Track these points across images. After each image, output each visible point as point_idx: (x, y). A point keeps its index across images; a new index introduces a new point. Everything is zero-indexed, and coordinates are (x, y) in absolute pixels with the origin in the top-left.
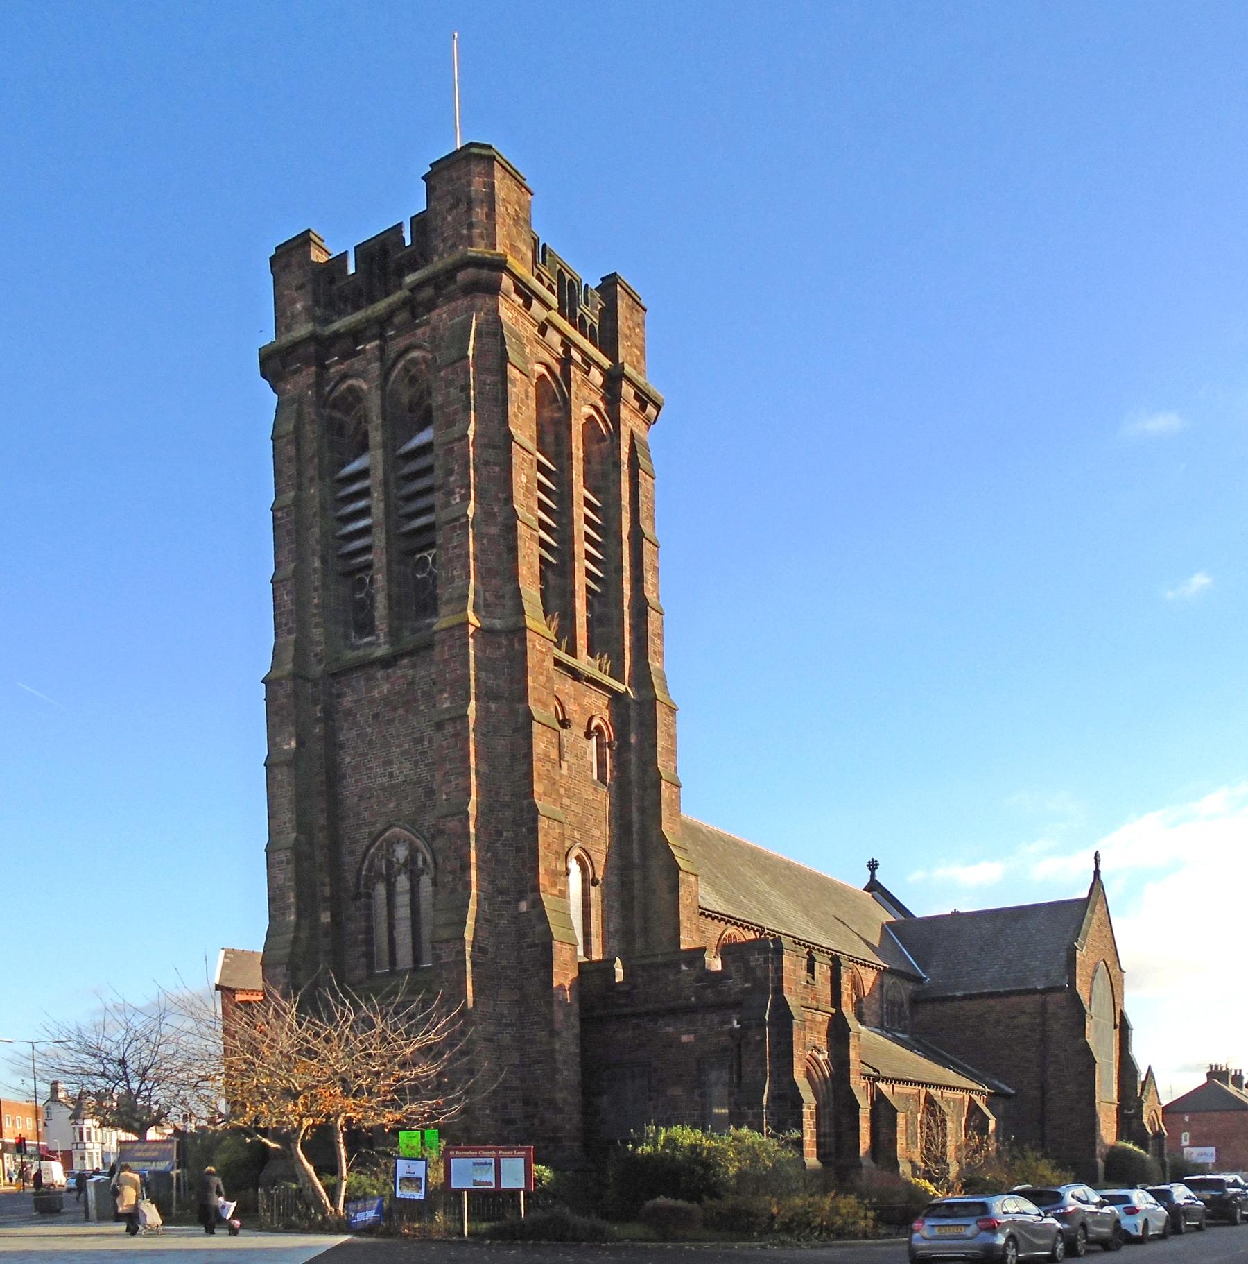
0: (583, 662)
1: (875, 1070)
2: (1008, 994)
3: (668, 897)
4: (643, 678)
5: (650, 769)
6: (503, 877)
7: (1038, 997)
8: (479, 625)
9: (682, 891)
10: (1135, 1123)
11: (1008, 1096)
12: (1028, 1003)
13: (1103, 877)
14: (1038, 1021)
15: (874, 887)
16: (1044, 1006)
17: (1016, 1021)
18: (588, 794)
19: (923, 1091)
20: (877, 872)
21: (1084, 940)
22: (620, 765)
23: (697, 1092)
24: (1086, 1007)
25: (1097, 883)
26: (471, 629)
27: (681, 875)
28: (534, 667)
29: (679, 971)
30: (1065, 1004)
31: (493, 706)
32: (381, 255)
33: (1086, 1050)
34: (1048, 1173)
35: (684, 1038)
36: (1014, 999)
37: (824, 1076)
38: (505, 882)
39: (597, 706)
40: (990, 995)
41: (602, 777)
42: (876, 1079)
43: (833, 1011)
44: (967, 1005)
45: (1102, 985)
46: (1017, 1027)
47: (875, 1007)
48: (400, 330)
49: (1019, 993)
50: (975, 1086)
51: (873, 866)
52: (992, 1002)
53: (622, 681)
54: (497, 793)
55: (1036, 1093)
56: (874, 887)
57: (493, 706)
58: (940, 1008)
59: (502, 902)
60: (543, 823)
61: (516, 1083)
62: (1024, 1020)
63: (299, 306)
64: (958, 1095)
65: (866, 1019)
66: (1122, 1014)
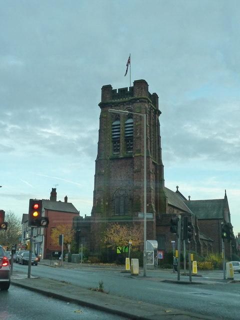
12: (215, 221)
15: (178, 192)
25: (226, 197)
32: (123, 91)
48: (127, 104)
51: (177, 187)
63: (107, 96)
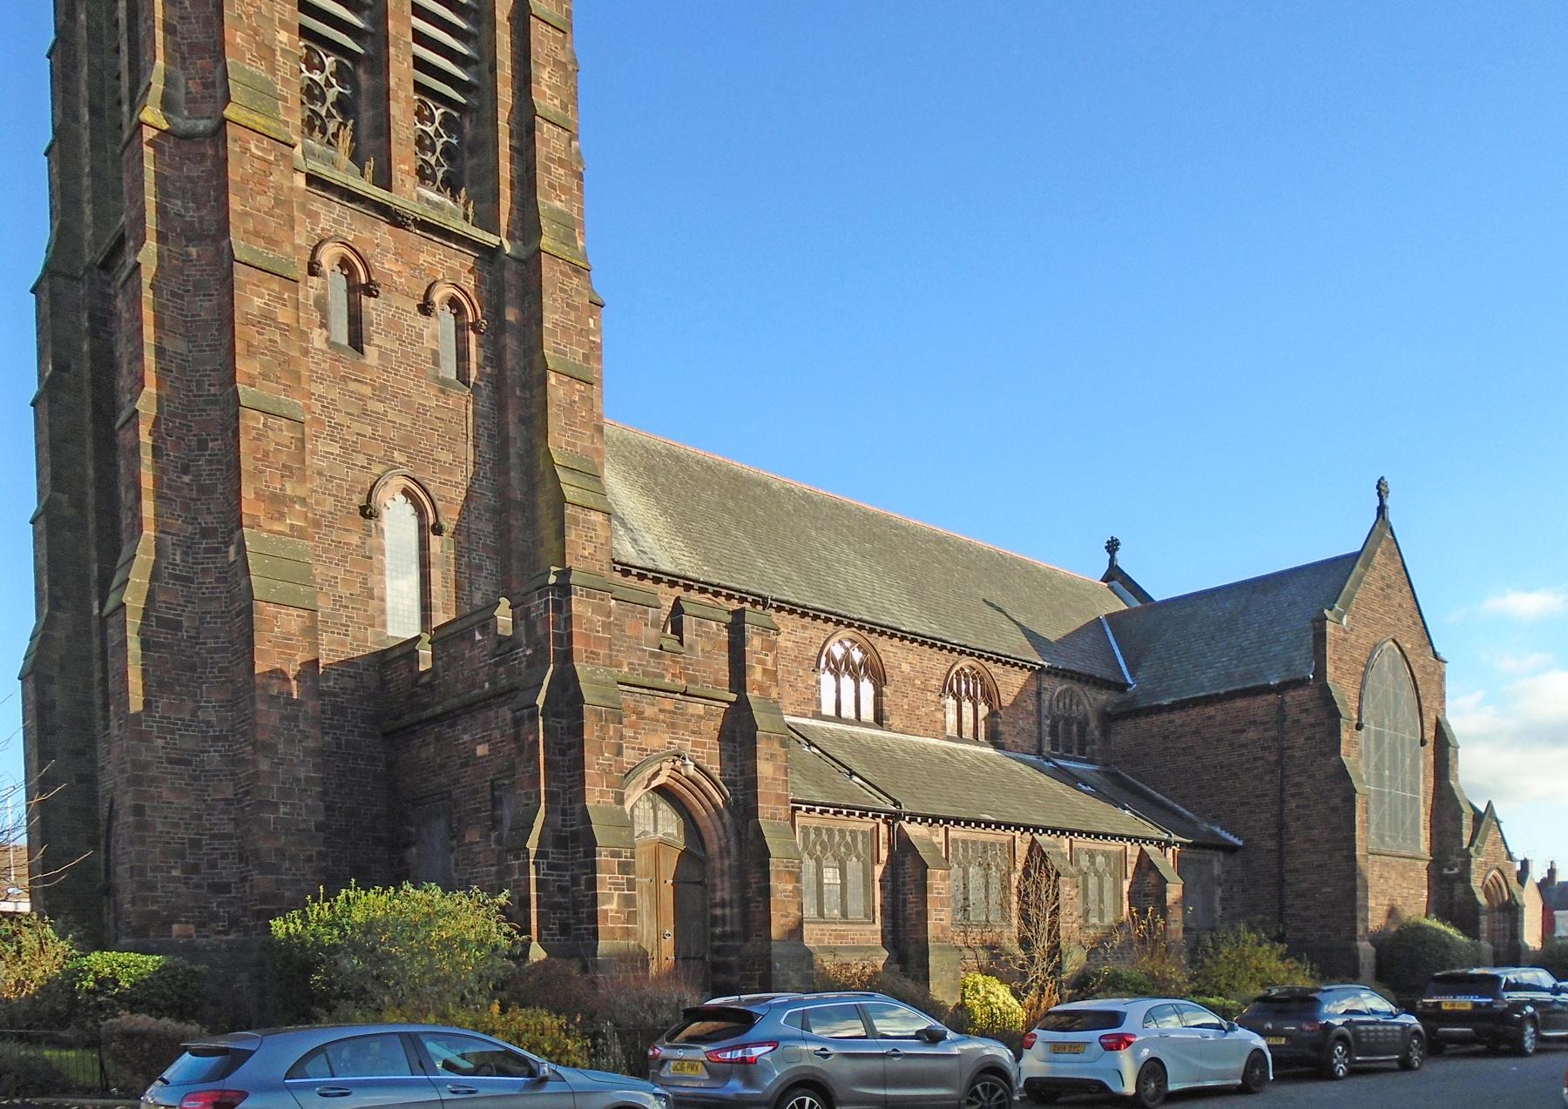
0: (410, 194)
1: (896, 803)
2: (1232, 696)
3: (555, 546)
4: (528, 223)
5: (537, 358)
6: (210, 513)
7: (1272, 698)
8: (165, 126)
9: (571, 535)
10: (1459, 888)
11: (1231, 849)
12: (1261, 705)
13: (1393, 516)
14: (1272, 733)
15: (1114, 575)
16: (1281, 708)
17: (1242, 738)
18: (428, 397)
19: (1133, 851)
20: (1118, 555)
21: (1346, 606)
22: (494, 358)
23: (493, 835)
24: (1348, 710)
26: (149, 133)
27: (569, 510)
28: (245, 180)
29: (473, 643)
30: (1310, 705)
31: (193, 251)
33: (1342, 775)
34: (1275, 964)
35: (482, 750)
36: (1240, 703)
37: (715, 806)
38: (210, 518)
39: (452, 271)
40: (1209, 700)
41: (462, 375)
42: (897, 816)
43: (733, 697)
44: (1178, 717)
45: (1388, 674)
46: (1244, 746)
47: (1028, 724)
49: (1246, 693)
50: (1155, 833)
51: (1113, 546)
52: (1210, 711)
53: (494, 230)
54: (199, 384)
55: (1271, 844)
56: (1114, 575)
57: (193, 251)
58: (1143, 723)
59: (206, 551)
60: (251, 422)
61: (229, 828)
62: (1252, 734)
64: (1114, 846)
65: (1007, 740)
66: (1440, 729)
